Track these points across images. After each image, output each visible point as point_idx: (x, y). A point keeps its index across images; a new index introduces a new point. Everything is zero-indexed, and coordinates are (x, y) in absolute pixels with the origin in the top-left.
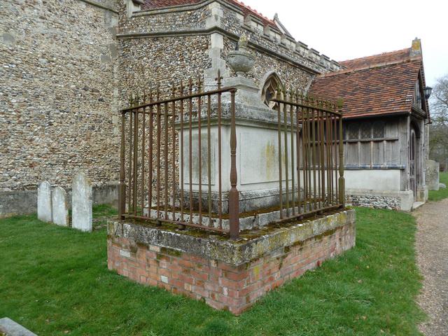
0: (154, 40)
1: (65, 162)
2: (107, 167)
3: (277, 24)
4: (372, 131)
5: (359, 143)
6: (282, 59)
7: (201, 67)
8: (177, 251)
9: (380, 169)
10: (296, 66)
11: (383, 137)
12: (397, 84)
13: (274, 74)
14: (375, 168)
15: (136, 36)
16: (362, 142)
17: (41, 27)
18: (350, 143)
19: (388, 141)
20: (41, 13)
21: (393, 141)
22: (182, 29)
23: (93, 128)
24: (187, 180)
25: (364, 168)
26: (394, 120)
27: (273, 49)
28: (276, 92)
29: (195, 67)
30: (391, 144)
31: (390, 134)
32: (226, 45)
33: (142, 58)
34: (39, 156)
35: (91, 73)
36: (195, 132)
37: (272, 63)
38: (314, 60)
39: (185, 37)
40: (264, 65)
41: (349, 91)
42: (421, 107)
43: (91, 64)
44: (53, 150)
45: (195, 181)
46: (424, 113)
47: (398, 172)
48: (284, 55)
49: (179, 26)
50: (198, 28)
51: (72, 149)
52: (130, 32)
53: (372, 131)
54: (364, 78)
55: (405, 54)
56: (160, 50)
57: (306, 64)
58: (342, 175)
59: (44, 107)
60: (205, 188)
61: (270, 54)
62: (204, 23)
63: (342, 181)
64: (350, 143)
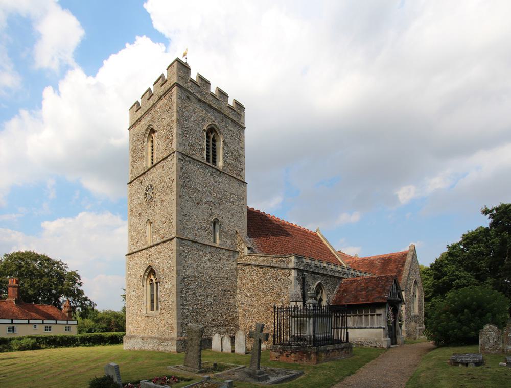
0: (260, 268)
1: (218, 325)
2: (234, 328)
3: (318, 234)
4: (370, 310)
5: (363, 316)
6: (324, 275)
7: (286, 283)
8: (441, 279)
9: (374, 328)
10: (331, 276)
11: (374, 313)
12: (382, 287)
13: (320, 283)
14: (371, 328)
15: (249, 265)
16: (365, 315)
17: (208, 265)
18: (359, 316)
19: (377, 315)
20: (208, 258)
21: (380, 315)
22: (276, 266)
23: (228, 309)
24: (293, 332)
25: (365, 328)
26: (381, 305)
27: (319, 271)
28: (321, 291)
29: (283, 283)
30: (379, 317)
31: (378, 312)
32: (298, 274)
33: (253, 275)
34: (208, 323)
35: (227, 282)
36: (296, 319)
37: (319, 277)
38: (341, 271)
39: (278, 269)
40: (315, 280)
41: (359, 289)
42: (397, 297)
43: (227, 278)
44: (213, 320)
45: (296, 332)
46: (399, 299)
47: (382, 330)
48: (325, 272)
49: (275, 264)
50: (285, 267)
51: (220, 319)
52: (246, 262)
53: (370, 310)
54: (367, 283)
55: (405, 255)
56: (264, 273)
57: (337, 275)
58: (347, 330)
59: (210, 300)
60: (305, 335)
61: (318, 273)
62: (288, 264)
63: (347, 333)
64: (359, 316)
